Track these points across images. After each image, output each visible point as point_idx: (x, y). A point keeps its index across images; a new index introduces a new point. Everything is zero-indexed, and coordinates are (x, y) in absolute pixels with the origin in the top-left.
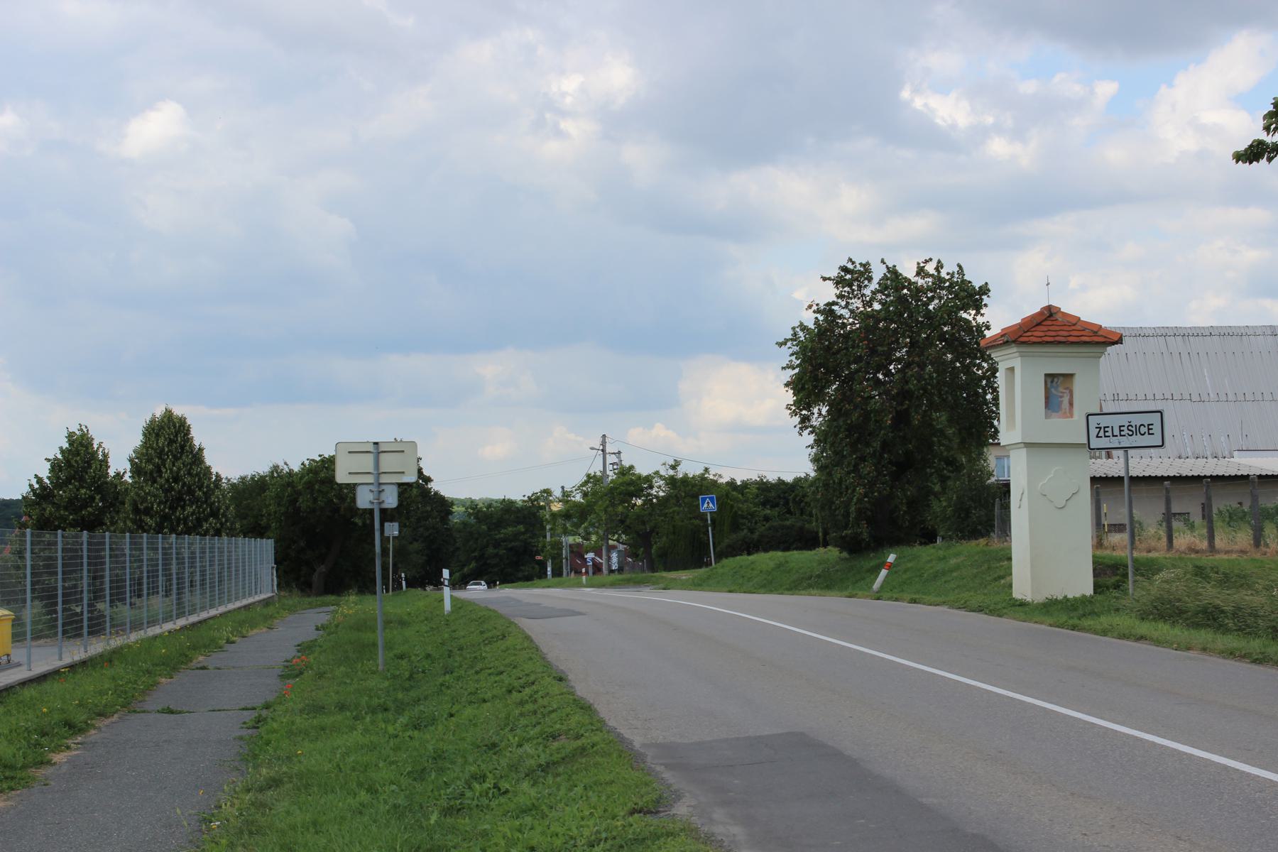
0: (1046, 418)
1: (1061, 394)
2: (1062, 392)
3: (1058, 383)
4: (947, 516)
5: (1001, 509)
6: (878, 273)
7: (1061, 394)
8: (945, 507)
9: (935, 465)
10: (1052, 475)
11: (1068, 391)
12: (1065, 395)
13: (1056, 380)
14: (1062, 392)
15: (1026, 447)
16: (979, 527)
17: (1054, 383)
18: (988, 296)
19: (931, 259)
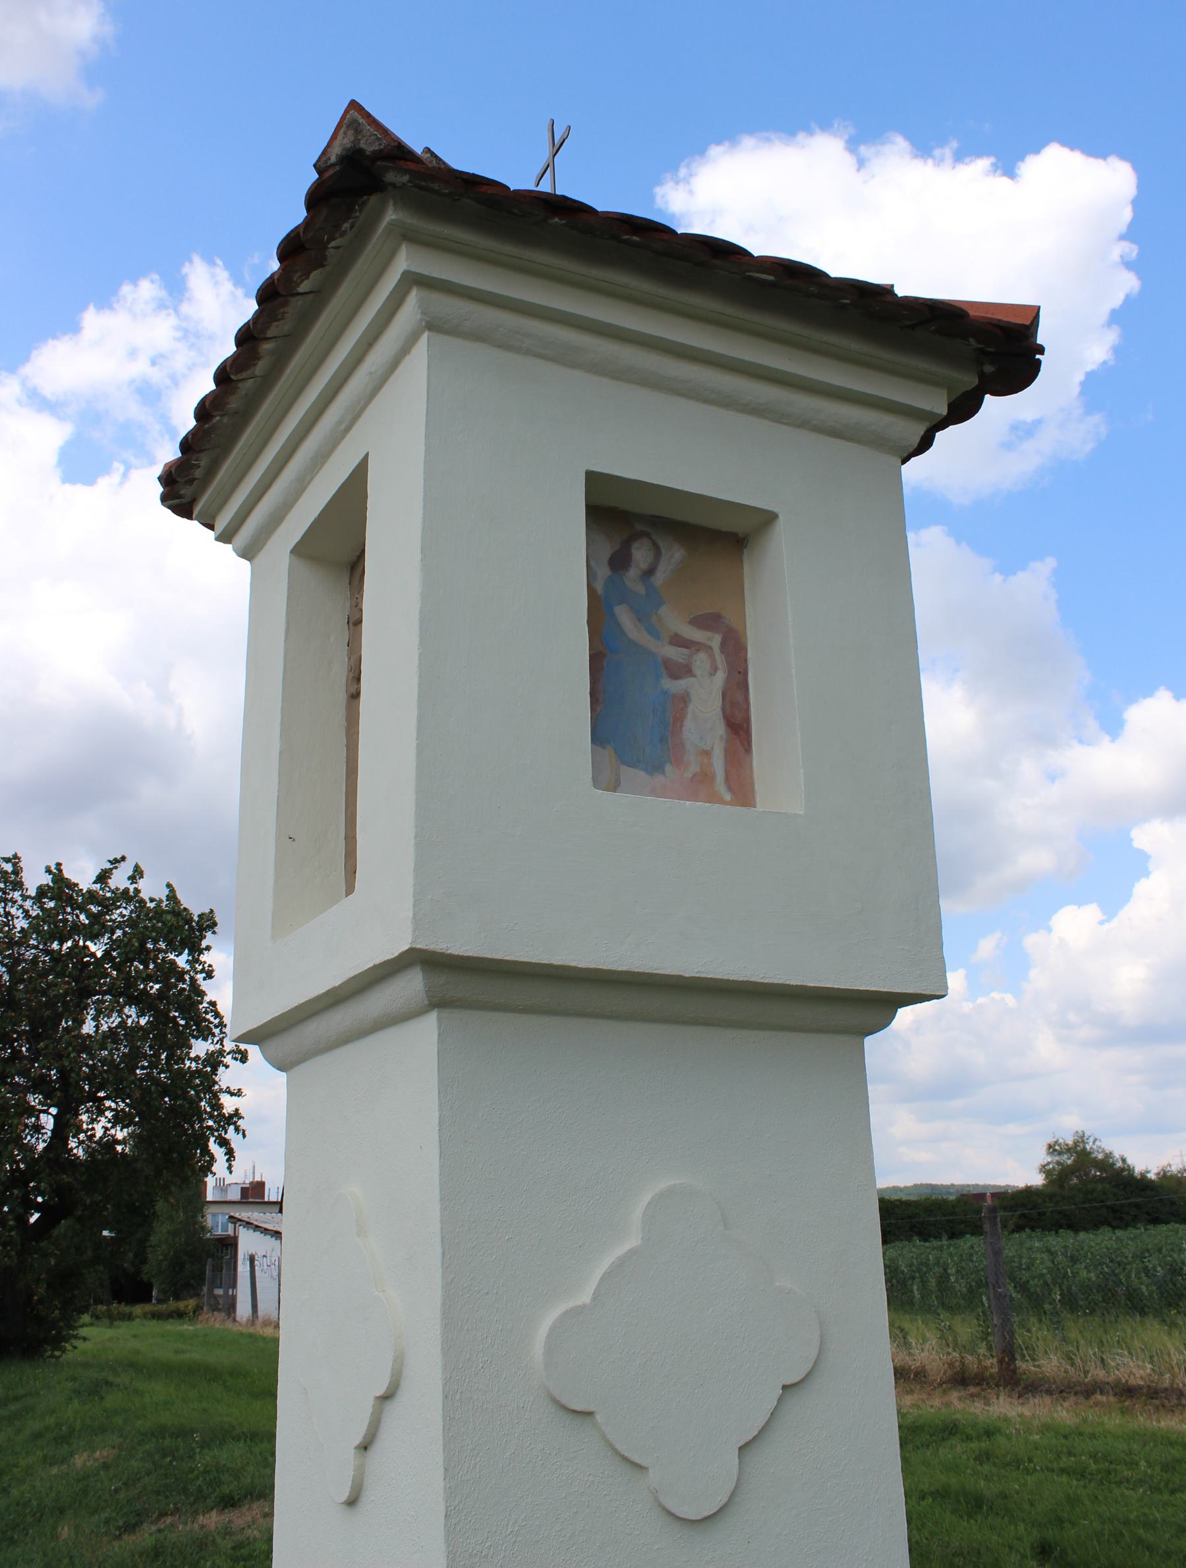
0: (1037, 309)
1: (675, 653)
2: (678, 641)
3: (660, 578)
4: (162, 1270)
5: (213, 1271)
6: (34, 878)
7: (675, 653)
8: (161, 1260)
9: (105, 1213)
10: (633, 1241)
11: (715, 640)
12: (700, 661)
13: (641, 555)
14: (678, 641)
15: (437, 1003)
16: (192, 1282)
17: (633, 573)
18: (214, 933)
19: (123, 858)
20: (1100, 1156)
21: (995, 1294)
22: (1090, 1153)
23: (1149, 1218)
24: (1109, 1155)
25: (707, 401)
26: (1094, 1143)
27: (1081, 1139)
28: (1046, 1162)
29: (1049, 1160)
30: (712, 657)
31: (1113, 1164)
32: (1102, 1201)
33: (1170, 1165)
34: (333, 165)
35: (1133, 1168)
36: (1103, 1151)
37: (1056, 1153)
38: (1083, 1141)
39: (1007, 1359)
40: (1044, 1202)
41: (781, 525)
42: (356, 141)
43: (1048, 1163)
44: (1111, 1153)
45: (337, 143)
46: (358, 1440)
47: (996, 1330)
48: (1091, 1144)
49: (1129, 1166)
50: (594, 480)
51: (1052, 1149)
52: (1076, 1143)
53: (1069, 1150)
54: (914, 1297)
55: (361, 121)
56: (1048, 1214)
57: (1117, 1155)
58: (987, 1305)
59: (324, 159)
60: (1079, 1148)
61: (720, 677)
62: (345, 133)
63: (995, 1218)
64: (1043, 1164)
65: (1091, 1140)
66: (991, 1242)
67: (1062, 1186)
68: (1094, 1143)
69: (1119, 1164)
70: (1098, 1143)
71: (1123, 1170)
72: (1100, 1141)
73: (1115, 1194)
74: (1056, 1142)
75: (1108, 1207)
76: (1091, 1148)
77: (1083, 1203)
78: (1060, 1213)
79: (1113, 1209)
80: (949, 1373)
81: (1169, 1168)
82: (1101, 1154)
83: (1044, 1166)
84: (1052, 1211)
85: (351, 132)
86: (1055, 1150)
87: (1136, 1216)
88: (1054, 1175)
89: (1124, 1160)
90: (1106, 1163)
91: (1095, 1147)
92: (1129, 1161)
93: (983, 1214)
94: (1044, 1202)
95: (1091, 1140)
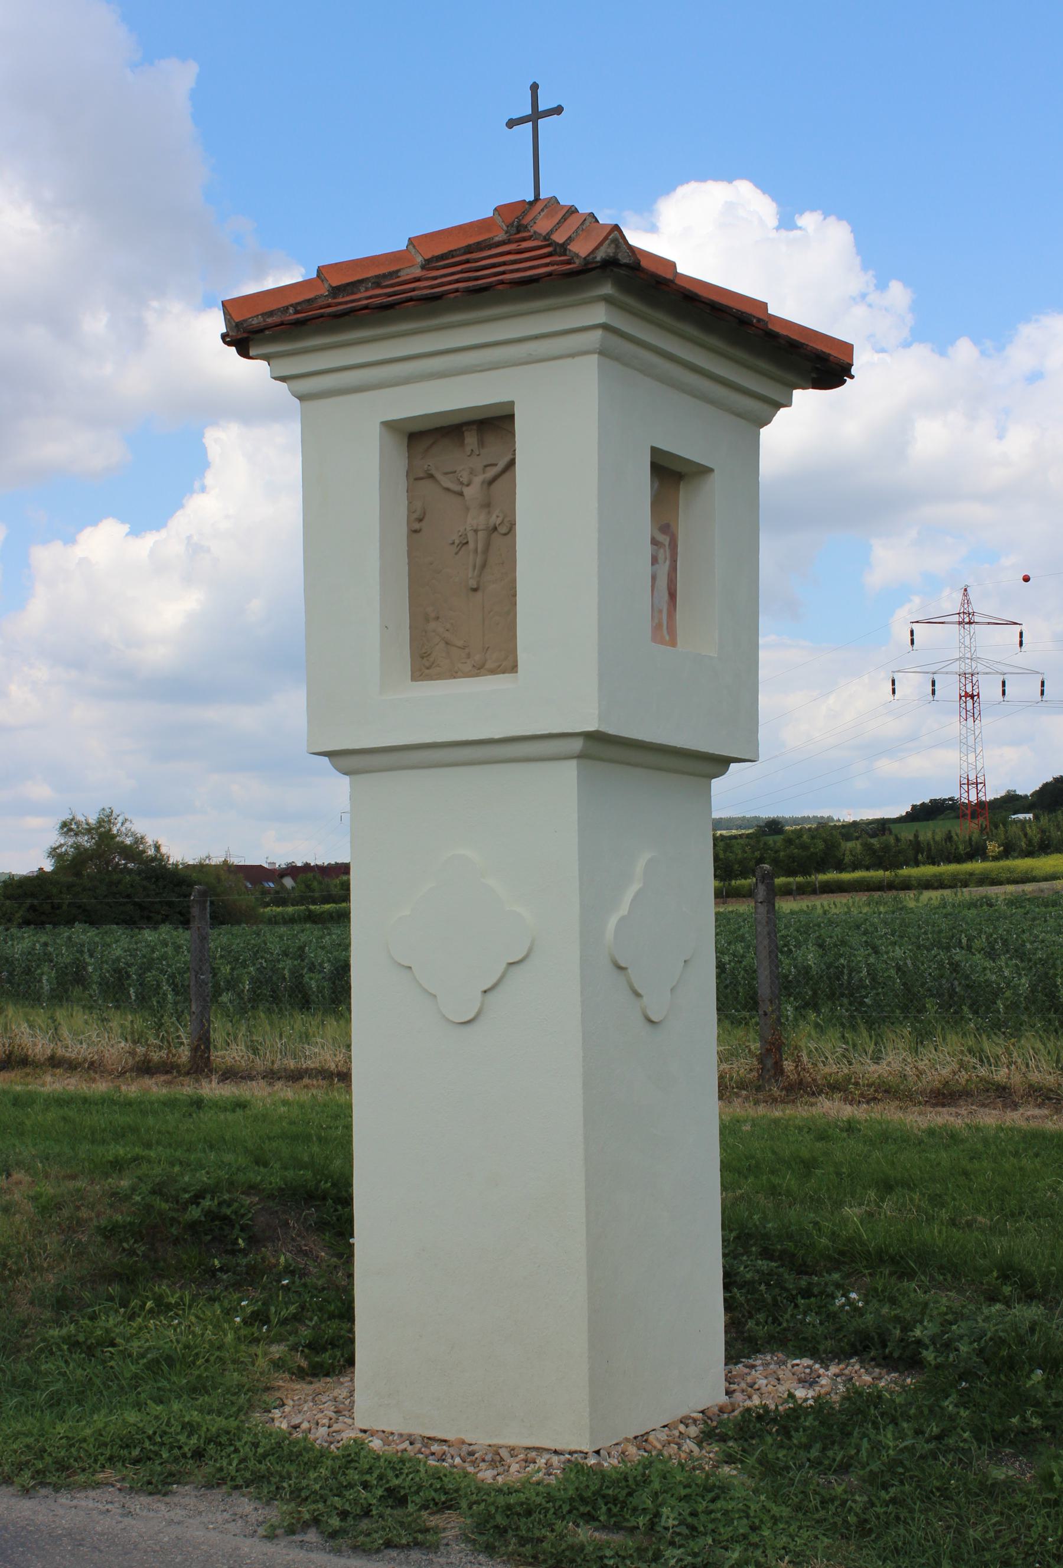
15: (581, 756)
20: (128, 841)
21: (196, 981)
22: (114, 837)
23: (182, 919)
24: (139, 840)
25: (695, 396)
26: (123, 824)
27: (106, 820)
28: (58, 844)
29: (62, 842)
30: (665, 551)
31: (144, 852)
32: (128, 896)
33: (209, 857)
34: (597, 262)
35: (168, 857)
36: (133, 835)
37: (72, 833)
38: (109, 821)
39: (202, 1047)
40: (61, 892)
41: (716, 479)
42: (616, 253)
43: (61, 846)
44: (142, 838)
45: (603, 249)
46: (485, 988)
47: (194, 1017)
48: (119, 825)
49: (162, 855)
50: (655, 451)
51: (66, 827)
52: (100, 822)
53: (89, 831)
54: (42, 988)
55: (621, 240)
56: (65, 907)
57: (150, 841)
58: (133, 998)
59: (591, 256)
60: (102, 829)
61: (668, 563)
62: (609, 245)
63: (205, 902)
64: (54, 846)
65: (120, 819)
66: (199, 928)
67: (78, 874)
68: (123, 824)
69: (151, 852)
70: (128, 825)
71: (153, 859)
72: (131, 822)
73: (145, 888)
74: (72, 820)
75: (135, 904)
76: (118, 830)
77: (106, 896)
78: (80, 907)
79: (140, 906)
80: (130, 1062)
81: (207, 862)
82: (131, 838)
83: (55, 849)
84: (69, 904)
85: (613, 246)
86: (71, 830)
87: (167, 916)
88: (68, 860)
89: (157, 847)
90: (133, 852)
91: (123, 829)
92: (163, 850)
93: (192, 898)
94: (61, 892)
95: (120, 819)
